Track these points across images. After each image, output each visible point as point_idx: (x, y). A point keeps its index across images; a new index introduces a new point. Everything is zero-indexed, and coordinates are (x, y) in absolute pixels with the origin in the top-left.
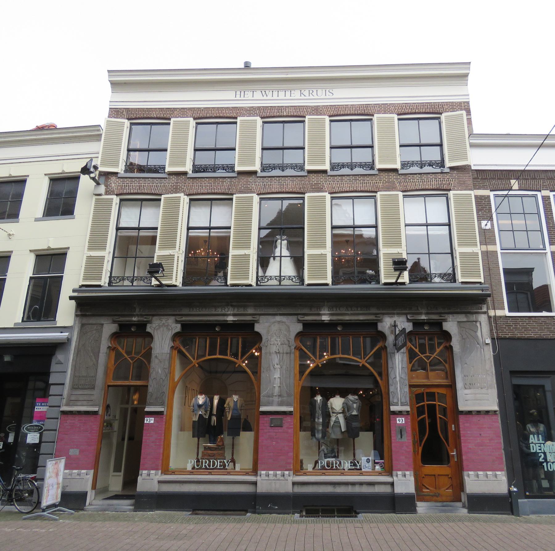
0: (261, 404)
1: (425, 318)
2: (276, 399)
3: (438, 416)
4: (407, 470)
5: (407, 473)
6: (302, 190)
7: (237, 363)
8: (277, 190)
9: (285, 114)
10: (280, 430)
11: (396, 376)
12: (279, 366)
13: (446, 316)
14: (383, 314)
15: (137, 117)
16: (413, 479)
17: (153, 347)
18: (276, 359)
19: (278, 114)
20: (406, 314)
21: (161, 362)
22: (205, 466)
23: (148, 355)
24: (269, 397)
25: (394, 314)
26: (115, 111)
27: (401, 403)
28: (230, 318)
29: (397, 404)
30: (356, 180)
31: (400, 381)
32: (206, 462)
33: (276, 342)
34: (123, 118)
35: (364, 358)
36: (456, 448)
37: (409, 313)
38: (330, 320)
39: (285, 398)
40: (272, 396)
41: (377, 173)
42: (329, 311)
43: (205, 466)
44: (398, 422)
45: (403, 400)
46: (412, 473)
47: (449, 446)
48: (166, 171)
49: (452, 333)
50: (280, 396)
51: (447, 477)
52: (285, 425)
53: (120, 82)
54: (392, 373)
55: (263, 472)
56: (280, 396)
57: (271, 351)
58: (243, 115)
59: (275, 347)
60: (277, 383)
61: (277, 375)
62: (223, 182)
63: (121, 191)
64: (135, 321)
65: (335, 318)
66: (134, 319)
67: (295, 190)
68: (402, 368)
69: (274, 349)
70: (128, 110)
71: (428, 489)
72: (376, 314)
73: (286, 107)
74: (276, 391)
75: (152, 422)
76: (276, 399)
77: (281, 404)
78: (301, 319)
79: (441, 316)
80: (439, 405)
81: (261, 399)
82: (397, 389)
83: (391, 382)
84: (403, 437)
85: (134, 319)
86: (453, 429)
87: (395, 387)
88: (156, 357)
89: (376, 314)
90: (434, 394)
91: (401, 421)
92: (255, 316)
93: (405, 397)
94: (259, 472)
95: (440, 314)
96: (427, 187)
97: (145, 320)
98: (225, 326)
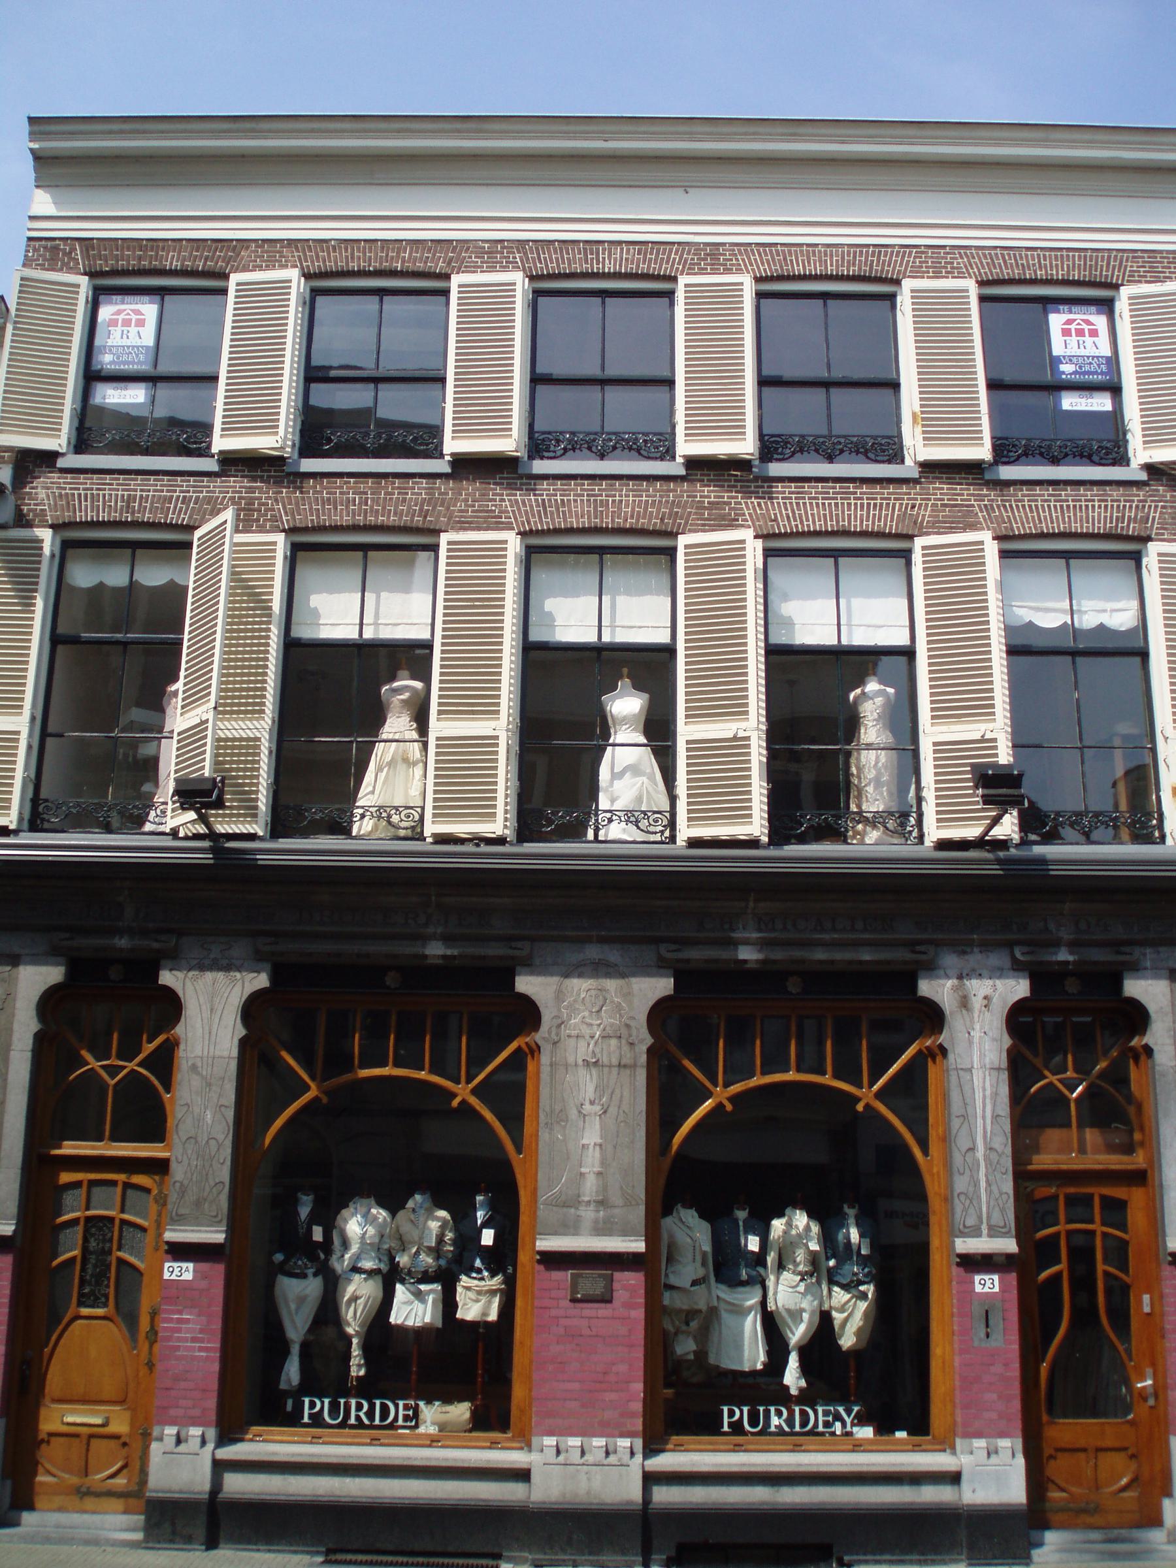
0: (539, 1228)
1: (1071, 958)
2: (588, 1214)
3: (1100, 1267)
4: (1003, 1435)
5: (1004, 1443)
6: (669, 524)
7: (454, 1095)
8: (585, 522)
9: (609, 267)
10: (602, 1310)
11: (974, 1142)
12: (597, 1108)
13: (1137, 951)
14: (937, 944)
15: (119, 273)
16: (1020, 1461)
17: (182, 1036)
18: (586, 1085)
19: (586, 267)
20: (1010, 945)
21: (209, 1085)
22: (358, 1418)
23: (164, 1062)
24: (565, 1205)
25: (971, 943)
26: (45, 248)
27: (991, 1228)
28: (436, 950)
29: (976, 1232)
30: (846, 495)
31: (986, 1158)
32: (359, 1407)
33: (586, 1031)
34: (70, 270)
35: (871, 1085)
36: (1153, 1364)
37: (1019, 943)
38: (764, 962)
39: (616, 1211)
40: (575, 1202)
41: (1143, 476)
42: (760, 930)
43: (358, 1418)
44: (978, 1288)
45: (997, 1219)
46: (1019, 1443)
47: (926, 1152)
48: (215, 449)
49: (1152, 1008)
50: (602, 1203)
51: (1123, 1454)
52: (620, 1295)
53: (70, 153)
54: (964, 1131)
55: (550, 1441)
56: (602, 1203)
57: (571, 1060)
58: (473, 269)
59: (582, 1044)
60: (591, 1163)
61: (591, 1136)
62: (403, 491)
63: (67, 516)
64: (121, 950)
65: (779, 955)
66: (123, 942)
67: (643, 523)
68: (996, 1117)
69: (582, 1051)
70: (86, 243)
71: (54, 1476)
72: (912, 945)
73: (611, 242)
74: (590, 1187)
75: (188, 1276)
76: (588, 1214)
77: (601, 1230)
78: (669, 955)
79: (1118, 953)
80: (1104, 1234)
81: (540, 1213)
82: (976, 1184)
83: (957, 1159)
84: (993, 1337)
85: (123, 942)
86: (1147, 1309)
87: (972, 1176)
88: (194, 1068)
89: (912, 945)
90: (1087, 1200)
91: (987, 1284)
92: (519, 944)
93: (1003, 1211)
94: (535, 1440)
95: (1116, 945)
96: (1076, 527)
97: (155, 945)
98: (421, 974)
